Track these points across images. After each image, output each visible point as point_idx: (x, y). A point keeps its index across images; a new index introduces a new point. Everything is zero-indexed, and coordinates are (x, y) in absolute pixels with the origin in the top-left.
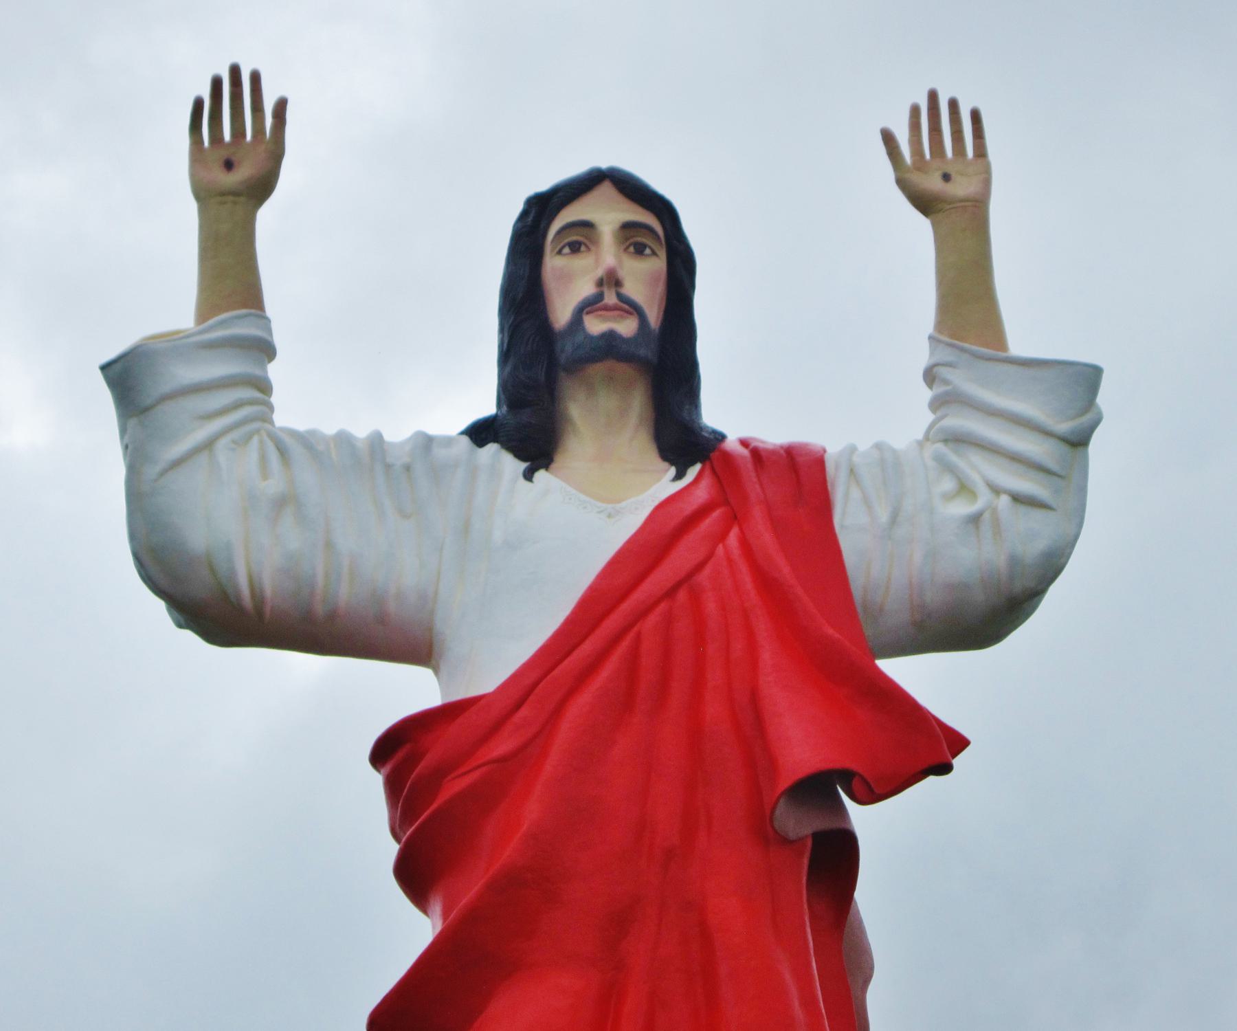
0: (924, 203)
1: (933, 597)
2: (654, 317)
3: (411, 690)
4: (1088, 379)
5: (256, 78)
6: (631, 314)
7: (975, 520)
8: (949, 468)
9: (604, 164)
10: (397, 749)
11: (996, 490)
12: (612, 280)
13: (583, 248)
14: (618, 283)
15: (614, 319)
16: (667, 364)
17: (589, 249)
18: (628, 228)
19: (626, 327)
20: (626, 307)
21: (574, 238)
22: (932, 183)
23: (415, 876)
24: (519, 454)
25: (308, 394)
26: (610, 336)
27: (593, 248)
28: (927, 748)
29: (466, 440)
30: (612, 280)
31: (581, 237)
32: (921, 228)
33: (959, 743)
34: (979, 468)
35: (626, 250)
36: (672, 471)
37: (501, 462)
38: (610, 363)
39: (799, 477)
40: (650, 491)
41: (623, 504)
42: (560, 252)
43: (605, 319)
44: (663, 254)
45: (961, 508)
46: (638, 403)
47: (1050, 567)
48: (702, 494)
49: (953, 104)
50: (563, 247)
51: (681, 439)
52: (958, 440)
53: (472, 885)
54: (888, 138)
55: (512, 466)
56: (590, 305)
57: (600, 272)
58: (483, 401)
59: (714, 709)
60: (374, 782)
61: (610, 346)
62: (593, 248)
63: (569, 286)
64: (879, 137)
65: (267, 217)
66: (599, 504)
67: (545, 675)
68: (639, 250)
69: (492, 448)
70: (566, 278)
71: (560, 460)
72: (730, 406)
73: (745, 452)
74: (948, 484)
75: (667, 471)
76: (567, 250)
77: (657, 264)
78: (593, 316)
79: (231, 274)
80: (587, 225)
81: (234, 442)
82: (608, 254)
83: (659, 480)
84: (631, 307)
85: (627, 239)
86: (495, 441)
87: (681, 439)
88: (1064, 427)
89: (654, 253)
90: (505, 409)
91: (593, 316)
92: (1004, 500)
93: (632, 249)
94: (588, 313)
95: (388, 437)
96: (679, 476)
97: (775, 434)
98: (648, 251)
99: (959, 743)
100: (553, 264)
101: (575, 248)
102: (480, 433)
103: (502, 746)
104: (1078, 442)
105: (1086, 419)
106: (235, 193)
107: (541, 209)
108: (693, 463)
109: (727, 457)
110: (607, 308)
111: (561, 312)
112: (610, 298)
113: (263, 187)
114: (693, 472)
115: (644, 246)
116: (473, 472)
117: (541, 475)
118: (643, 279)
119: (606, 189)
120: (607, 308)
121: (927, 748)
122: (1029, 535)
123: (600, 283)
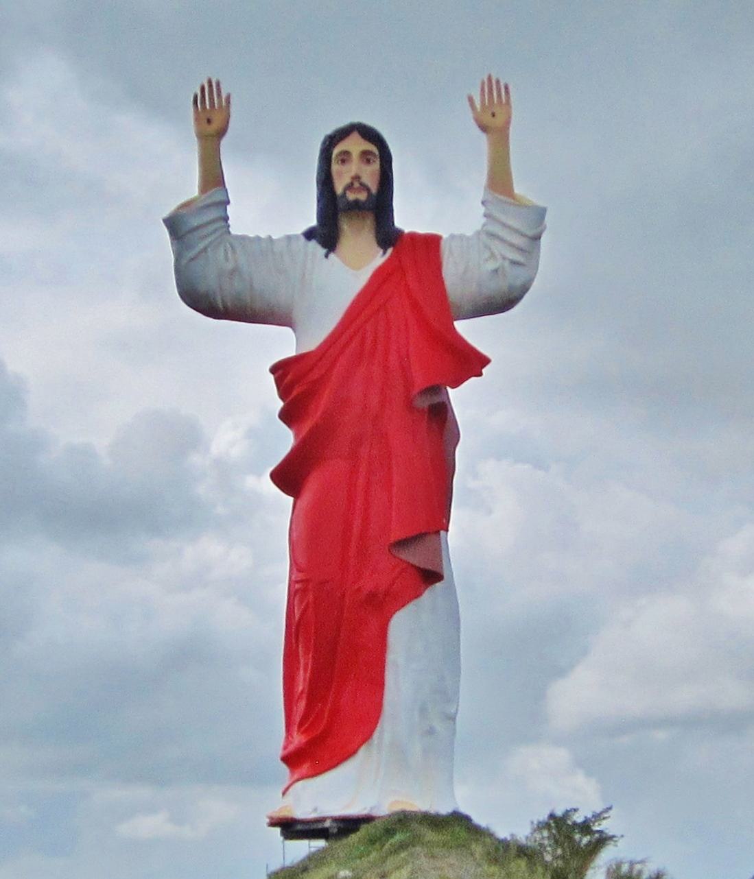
0: (484, 128)
2: (374, 190)
3: (284, 343)
4: (541, 213)
5: (218, 84)
7: (496, 271)
8: (487, 247)
9: (356, 119)
10: (281, 370)
11: (504, 258)
16: (379, 206)
19: (362, 196)
22: (487, 119)
23: (287, 416)
25: (244, 219)
26: (356, 202)
28: (471, 363)
29: (303, 239)
31: (345, 157)
32: (483, 140)
33: (485, 361)
34: (498, 248)
36: (381, 251)
37: (315, 248)
39: (430, 245)
45: (491, 265)
47: (525, 289)
49: (498, 82)
51: (387, 235)
52: (492, 235)
53: (307, 426)
54: (471, 99)
55: (323, 251)
56: (350, 187)
58: (311, 220)
59: (393, 360)
61: (356, 206)
64: (467, 100)
65: (225, 143)
68: (368, 161)
70: (340, 174)
72: (405, 219)
74: (487, 254)
75: (378, 252)
77: (376, 166)
78: (353, 198)
79: (213, 178)
84: (364, 187)
87: (387, 235)
88: (531, 233)
89: (374, 161)
91: (353, 198)
92: (507, 264)
95: (274, 237)
96: (384, 253)
99: (485, 361)
100: (335, 167)
101: (343, 161)
102: (310, 235)
103: (315, 375)
104: (537, 238)
105: (539, 230)
106: (212, 136)
107: (332, 141)
108: (389, 247)
111: (339, 189)
112: (356, 185)
113: (222, 132)
114: (390, 251)
117: (332, 256)
121: (471, 363)
122: (516, 277)
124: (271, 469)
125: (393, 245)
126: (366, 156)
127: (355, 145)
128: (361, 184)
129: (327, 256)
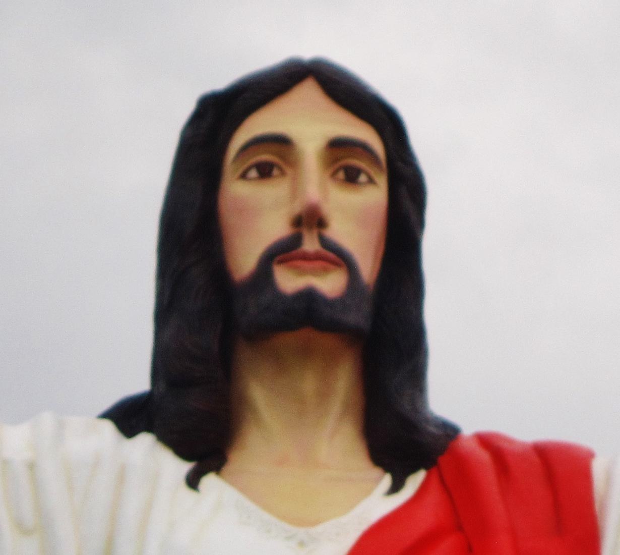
2: (368, 267)
6: (336, 264)
9: (307, 52)
13: (276, 172)
15: (314, 273)
16: (381, 336)
17: (283, 173)
18: (338, 147)
19: (330, 284)
20: (331, 255)
21: (265, 157)
24: (182, 450)
26: (309, 296)
27: (289, 171)
30: (311, 219)
35: (334, 175)
36: (387, 481)
38: (305, 333)
40: (358, 510)
41: (319, 529)
42: (244, 176)
43: (302, 272)
44: (382, 181)
46: (344, 381)
48: (427, 518)
56: (284, 251)
57: (297, 208)
61: (308, 310)
62: (289, 171)
63: (256, 217)
66: (288, 526)
68: (351, 177)
69: (145, 441)
71: (237, 460)
72: (471, 384)
73: (484, 456)
75: (378, 481)
76: (253, 173)
77: (374, 196)
82: (314, 183)
83: (368, 493)
84: (337, 257)
85: (336, 160)
86: (149, 429)
87: (399, 434)
89: (371, 181)
90: (162, 386)
93: (341, 175)
94: (281, 262)
96: (396, 488)
97: (524, 428)
98: (363, 178)
100: (238, 191)
101: (265, 171)
102: (129, 417)
107: (218, 116)
108: (414, 470)
109: (462, 463)
111: (245, 259)
112: (310, 244)
114: (414, 482)
116: (121, 477)
117: (210, 481)
118: (355, 217)
119: (309, 91)
120: (306, 257)
123: (298, 222)
124: (602, 469)
125: (427, 468)
126: (342, 159)
127: (309, 122)
128: (325, 243)
129: (193, 481)
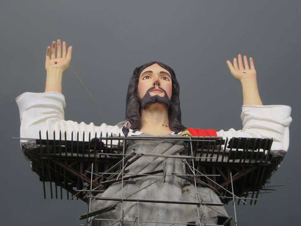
1: (171, 185)
12: (157, 83)
14: (159, 85)
19: (162, 95)
30: (157, 83)
44: (171, 81)
50: (144, 78)
56: (151, 89)
60: (35, 173)
61: (156, 100)
67: (167, 150)
68: (165, 78)
80: (151, 72)
81: (52, 120)
84: (163, 90)
94: (151, 92)
98: (167, 79)
101: (147, 77)
110: (156, 90)
112: (157, 87)
115: (166, 78)
118: (166, 84)
123: (154, 84)
